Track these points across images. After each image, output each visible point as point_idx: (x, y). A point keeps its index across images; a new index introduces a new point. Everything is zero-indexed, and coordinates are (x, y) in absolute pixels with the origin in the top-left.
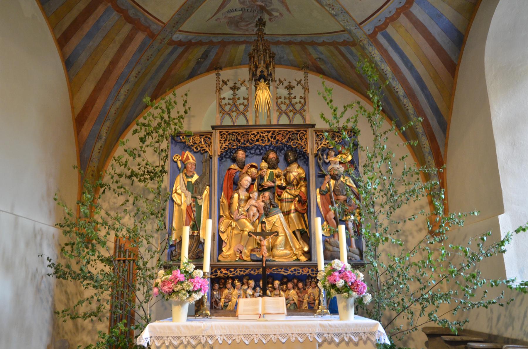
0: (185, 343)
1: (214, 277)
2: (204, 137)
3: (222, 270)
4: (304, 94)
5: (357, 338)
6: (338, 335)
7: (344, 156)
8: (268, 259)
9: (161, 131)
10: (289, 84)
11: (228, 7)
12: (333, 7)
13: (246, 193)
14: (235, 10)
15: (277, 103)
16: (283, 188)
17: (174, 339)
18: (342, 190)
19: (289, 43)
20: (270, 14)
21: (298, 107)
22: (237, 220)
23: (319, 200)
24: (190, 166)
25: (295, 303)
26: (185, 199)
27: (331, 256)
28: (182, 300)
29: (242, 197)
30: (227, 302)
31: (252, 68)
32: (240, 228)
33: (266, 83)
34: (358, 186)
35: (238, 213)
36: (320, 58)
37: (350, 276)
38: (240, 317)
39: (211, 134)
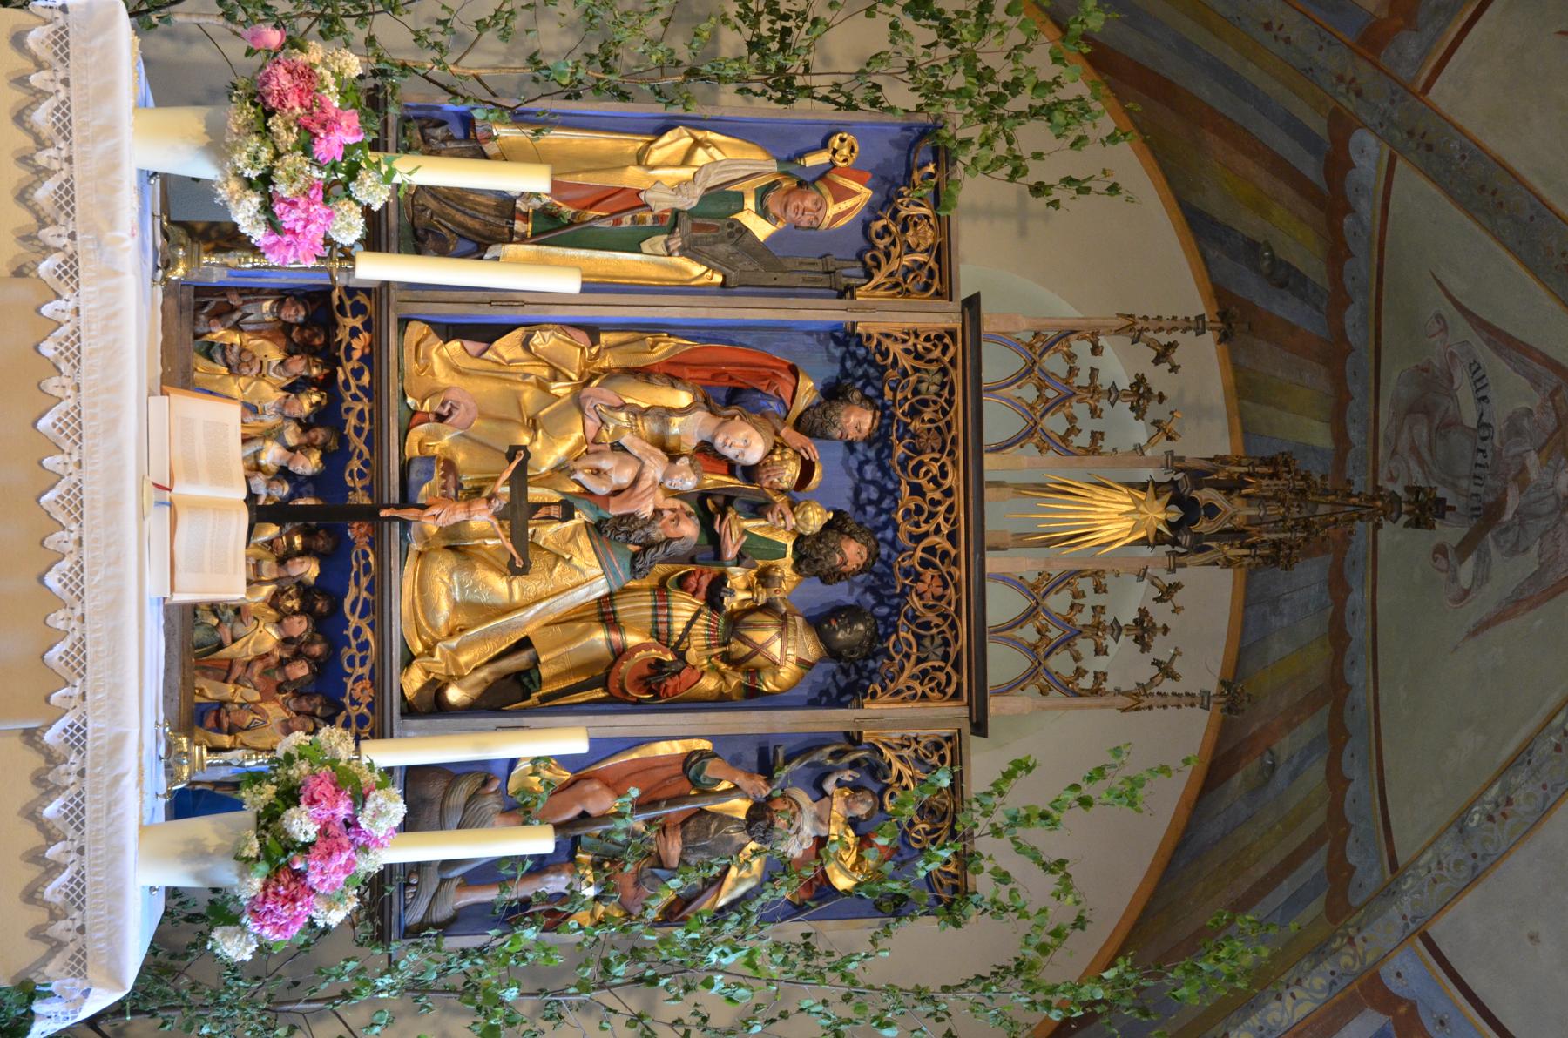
0: (42, 158)
1: (336, 302)
2: (932, 264)
3: (365, 337)
4: (1118, 691)
5: (59, 899)
6: (76, 814)
7: (850, 858)
8: (414, 526)
9: (957, 81)
10: (1159, 625)
11: (1498, 367)
12: (1497, 815)
13: (694, 444)
14: (1484, 398)
15: (1080, 573)
16: (714, 596)
17: (57, 109)
18: (703, 849)
19: (1338, 636)
20: (1466, 547)
21: (1061, 663)
22: (577, 403)
23: (663, 749)
24: (808, 203)
25: (221, 646)
26: (669, 183)
27: (425, 801)
28: (234, 147)
29: (676, 425)
30: (225, 358)
31: (1228, 468)
32: (545, 416)
33: (1162, 527)
34: (721, 914)
35: (610, 408)
36: (1273, 768)
37: (333, 865)
38: (159, 403)
39: (945, 294)
